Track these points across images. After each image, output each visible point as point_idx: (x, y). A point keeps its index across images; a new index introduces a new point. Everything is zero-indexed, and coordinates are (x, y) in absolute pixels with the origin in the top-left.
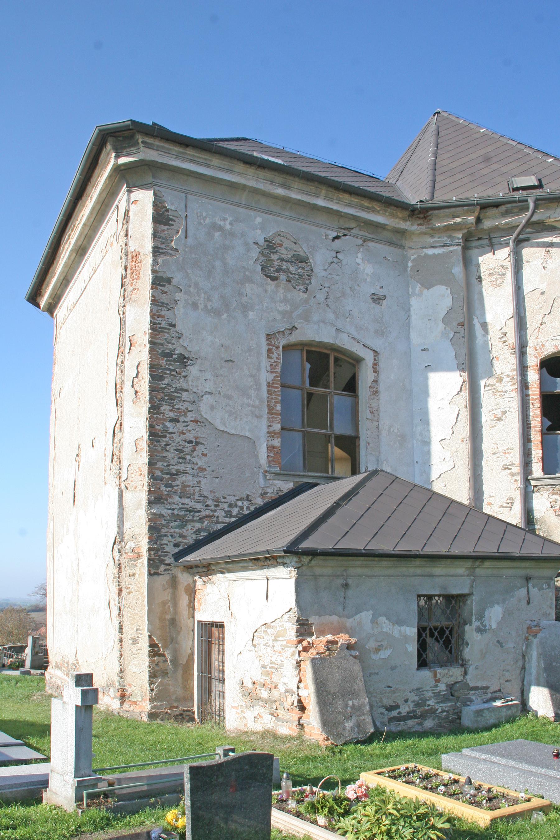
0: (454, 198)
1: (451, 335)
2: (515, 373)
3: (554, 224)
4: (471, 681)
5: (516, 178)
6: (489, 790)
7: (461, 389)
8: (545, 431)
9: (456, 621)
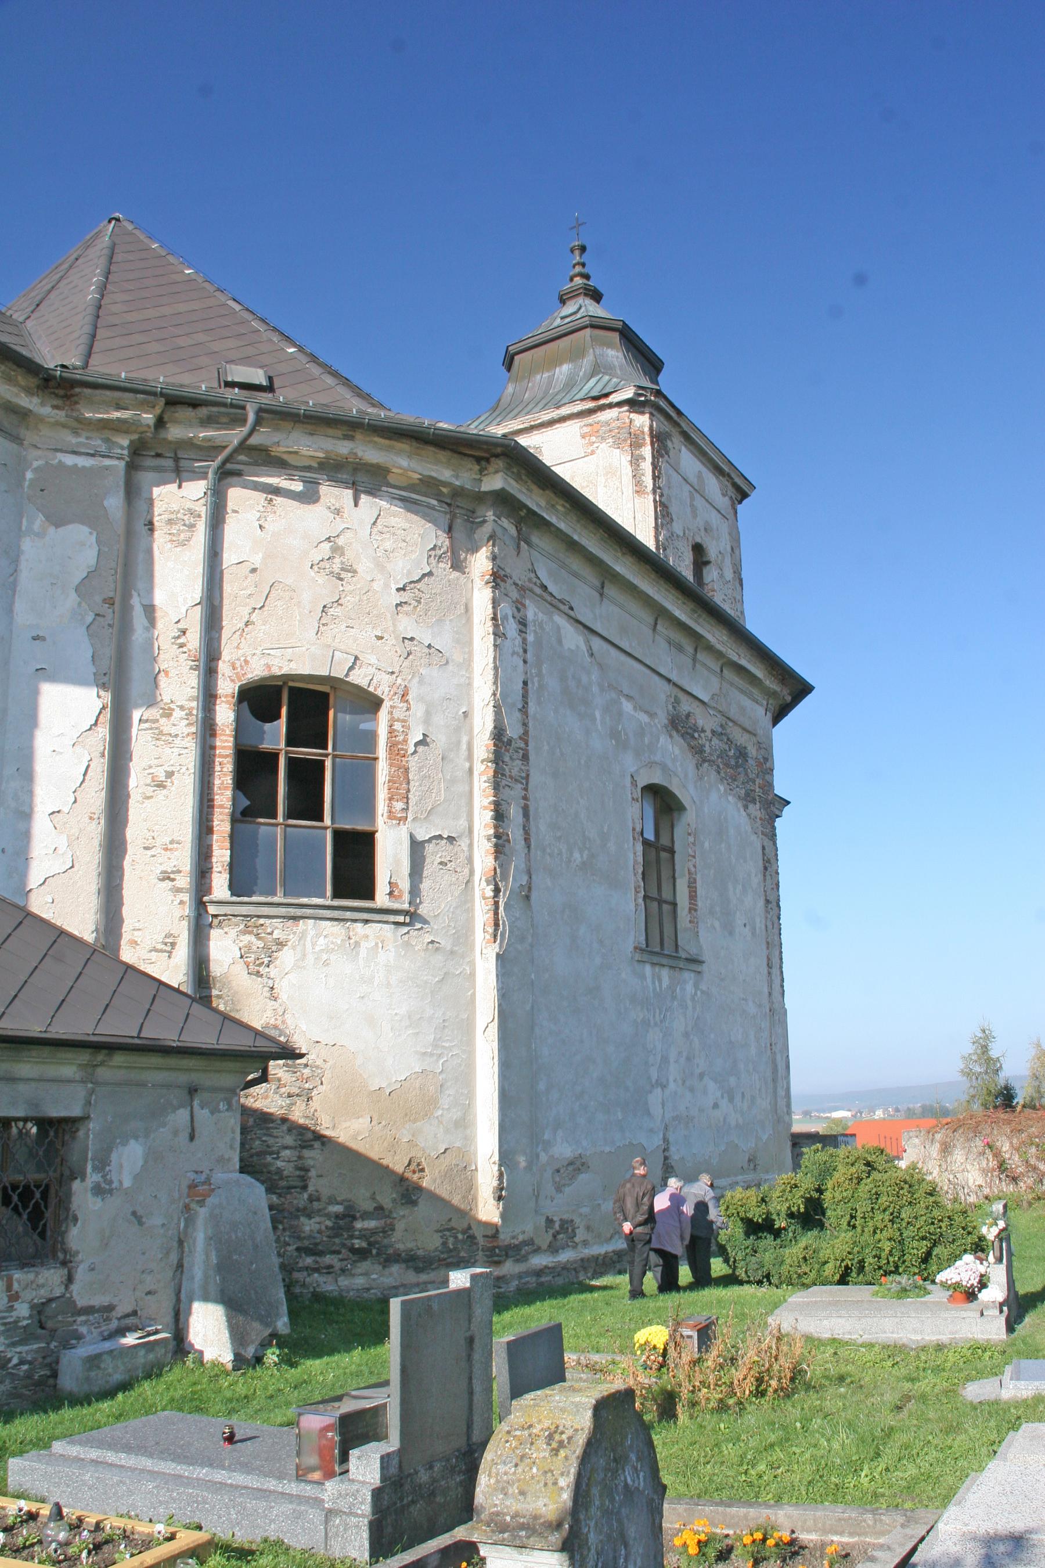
0: (123, 375)
1: (90, 618)
2: (194, 704)
3: (285, 457)
4: (81, 1295)
5: (233, 367)
6: (98, 1527)
7: (97, 721)
8: (238, 815)
9: (55, 1171)
